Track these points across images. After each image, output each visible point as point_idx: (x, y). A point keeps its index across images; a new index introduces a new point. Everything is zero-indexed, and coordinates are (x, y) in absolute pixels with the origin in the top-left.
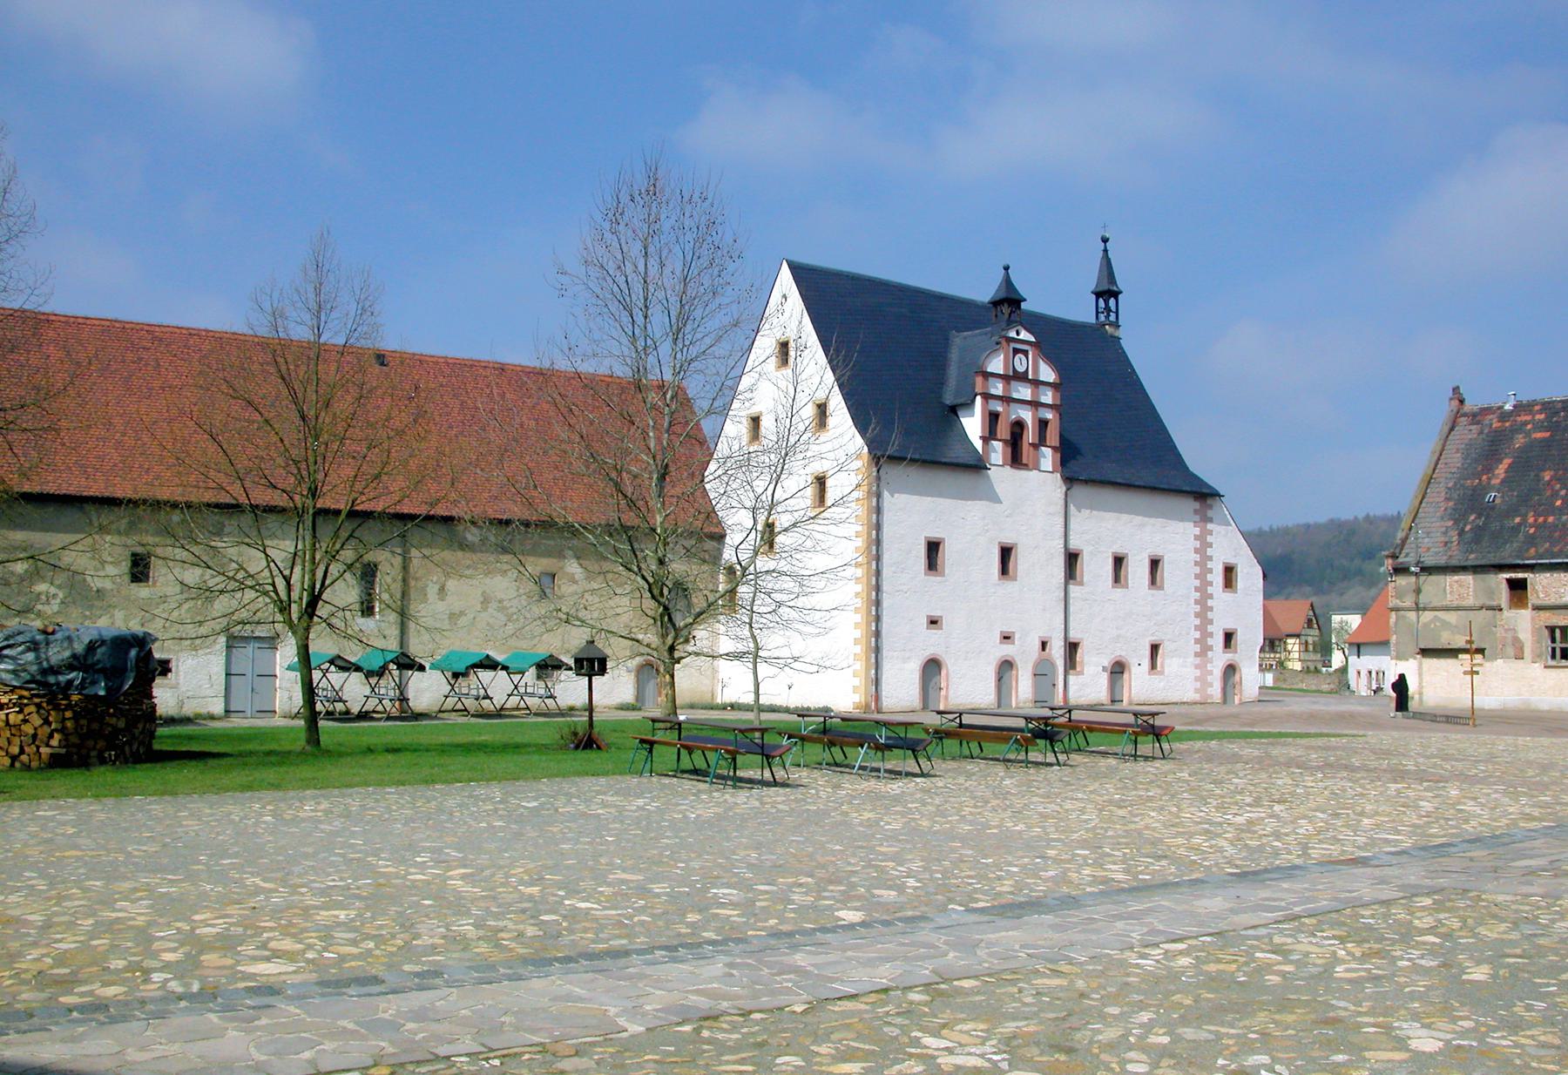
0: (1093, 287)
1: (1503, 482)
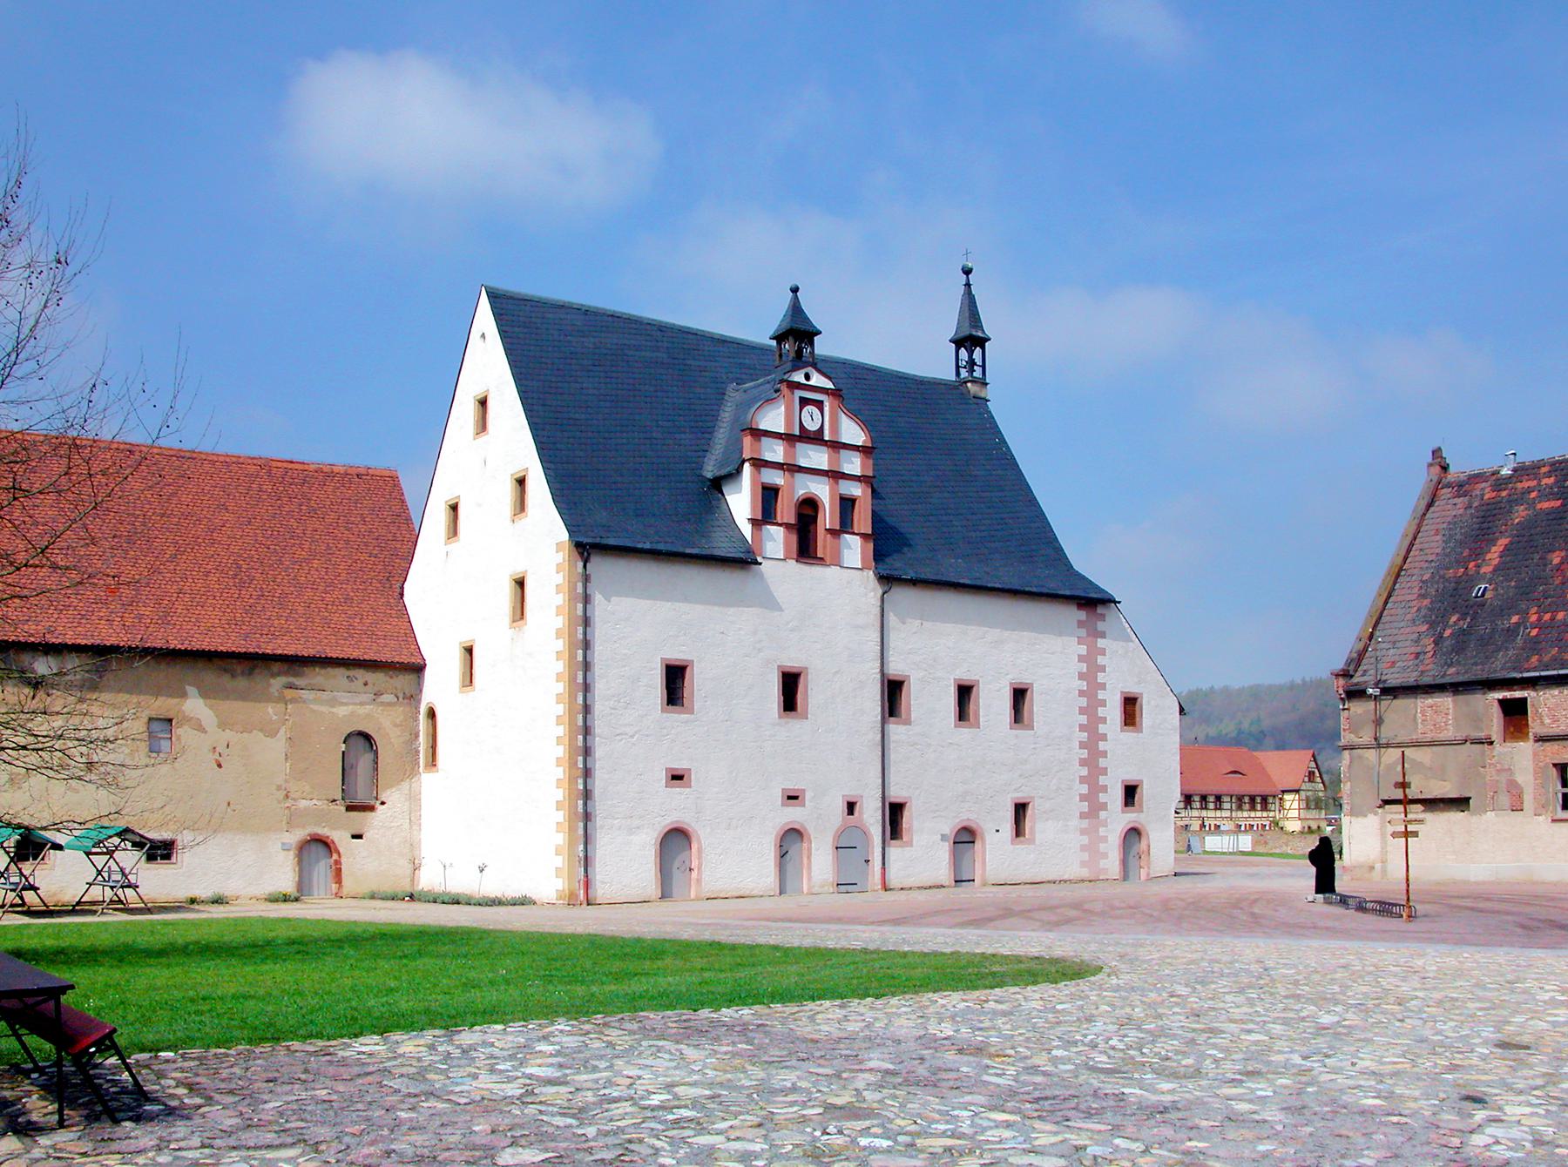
0: (951, 334)
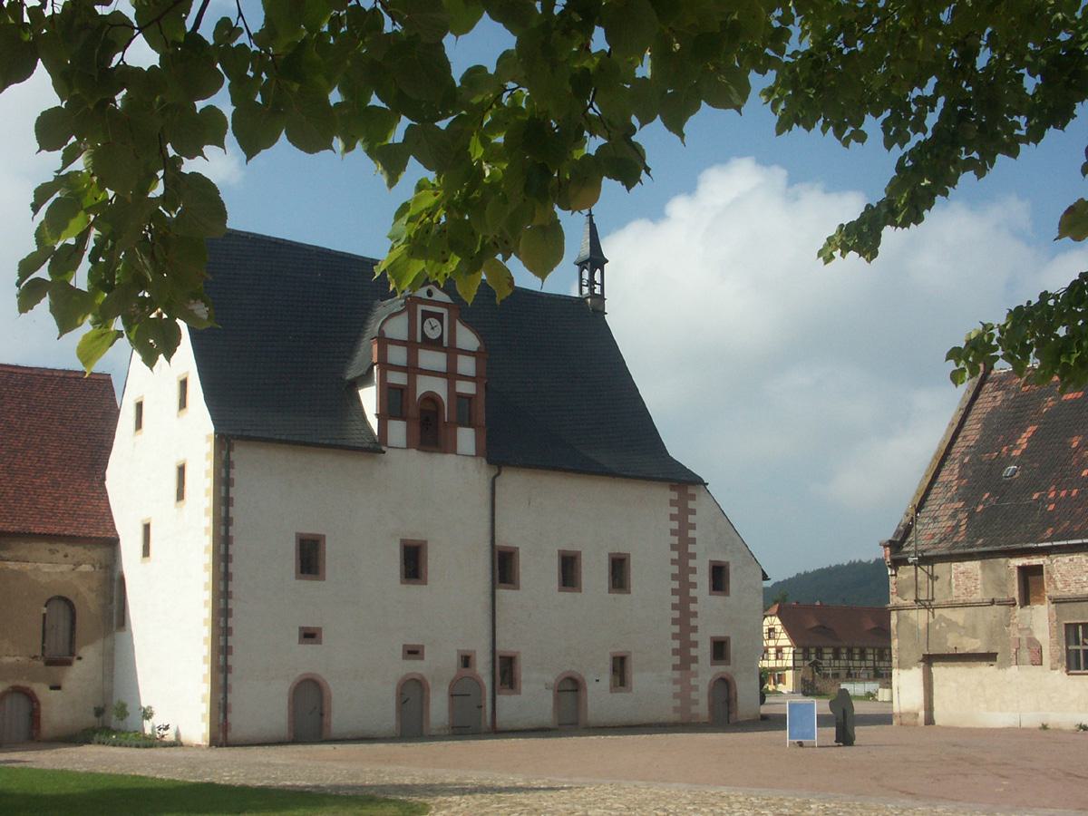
1: (1024, 452)
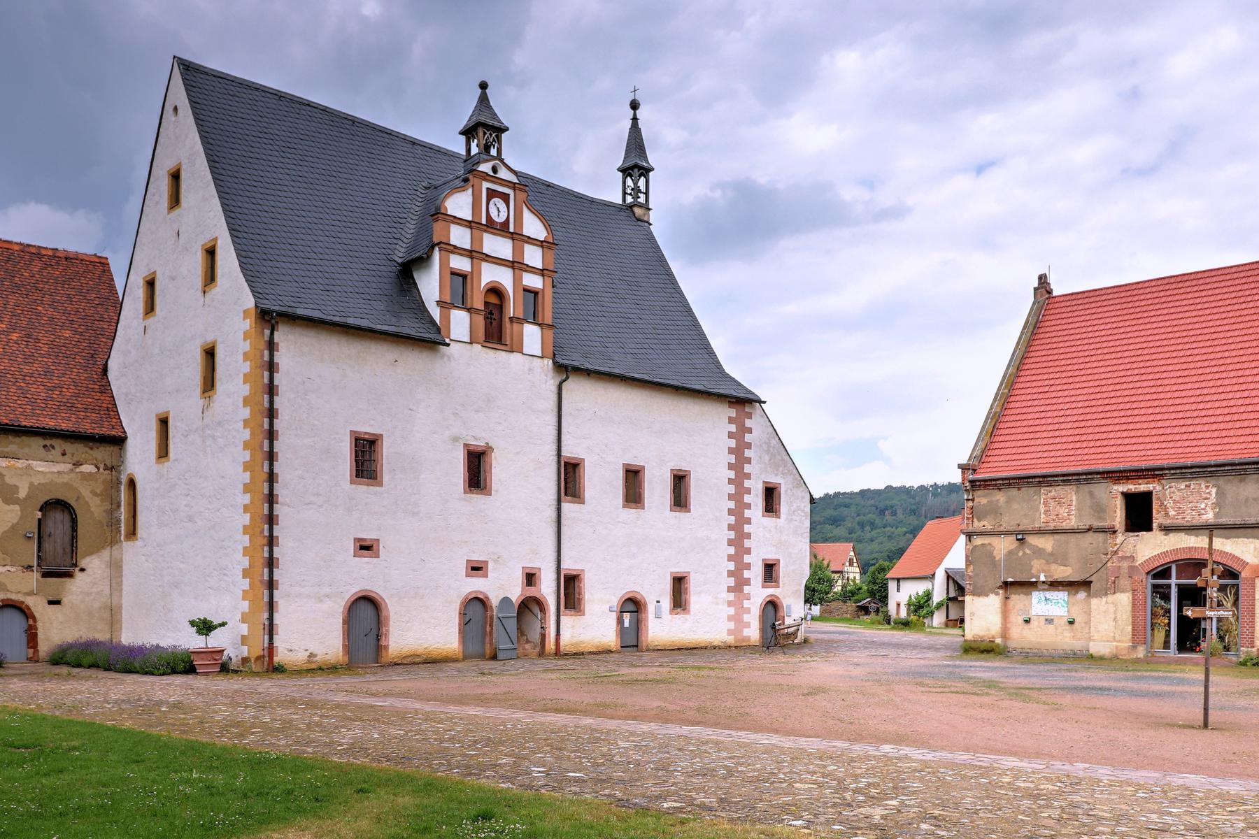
0: (619, 163)
